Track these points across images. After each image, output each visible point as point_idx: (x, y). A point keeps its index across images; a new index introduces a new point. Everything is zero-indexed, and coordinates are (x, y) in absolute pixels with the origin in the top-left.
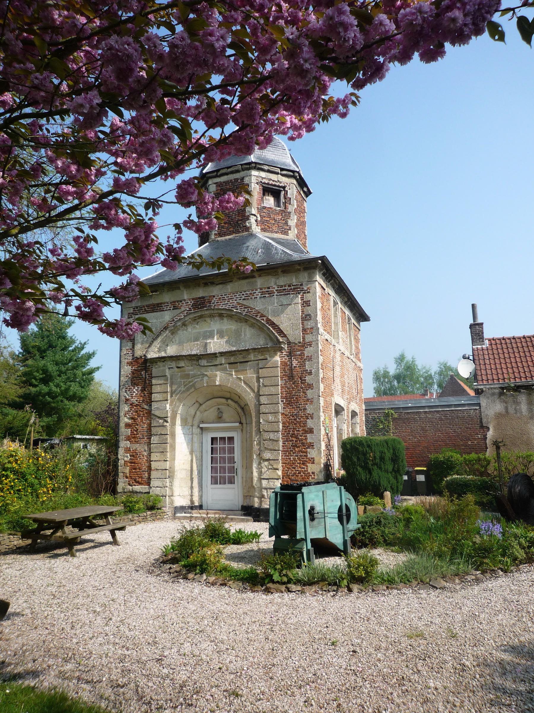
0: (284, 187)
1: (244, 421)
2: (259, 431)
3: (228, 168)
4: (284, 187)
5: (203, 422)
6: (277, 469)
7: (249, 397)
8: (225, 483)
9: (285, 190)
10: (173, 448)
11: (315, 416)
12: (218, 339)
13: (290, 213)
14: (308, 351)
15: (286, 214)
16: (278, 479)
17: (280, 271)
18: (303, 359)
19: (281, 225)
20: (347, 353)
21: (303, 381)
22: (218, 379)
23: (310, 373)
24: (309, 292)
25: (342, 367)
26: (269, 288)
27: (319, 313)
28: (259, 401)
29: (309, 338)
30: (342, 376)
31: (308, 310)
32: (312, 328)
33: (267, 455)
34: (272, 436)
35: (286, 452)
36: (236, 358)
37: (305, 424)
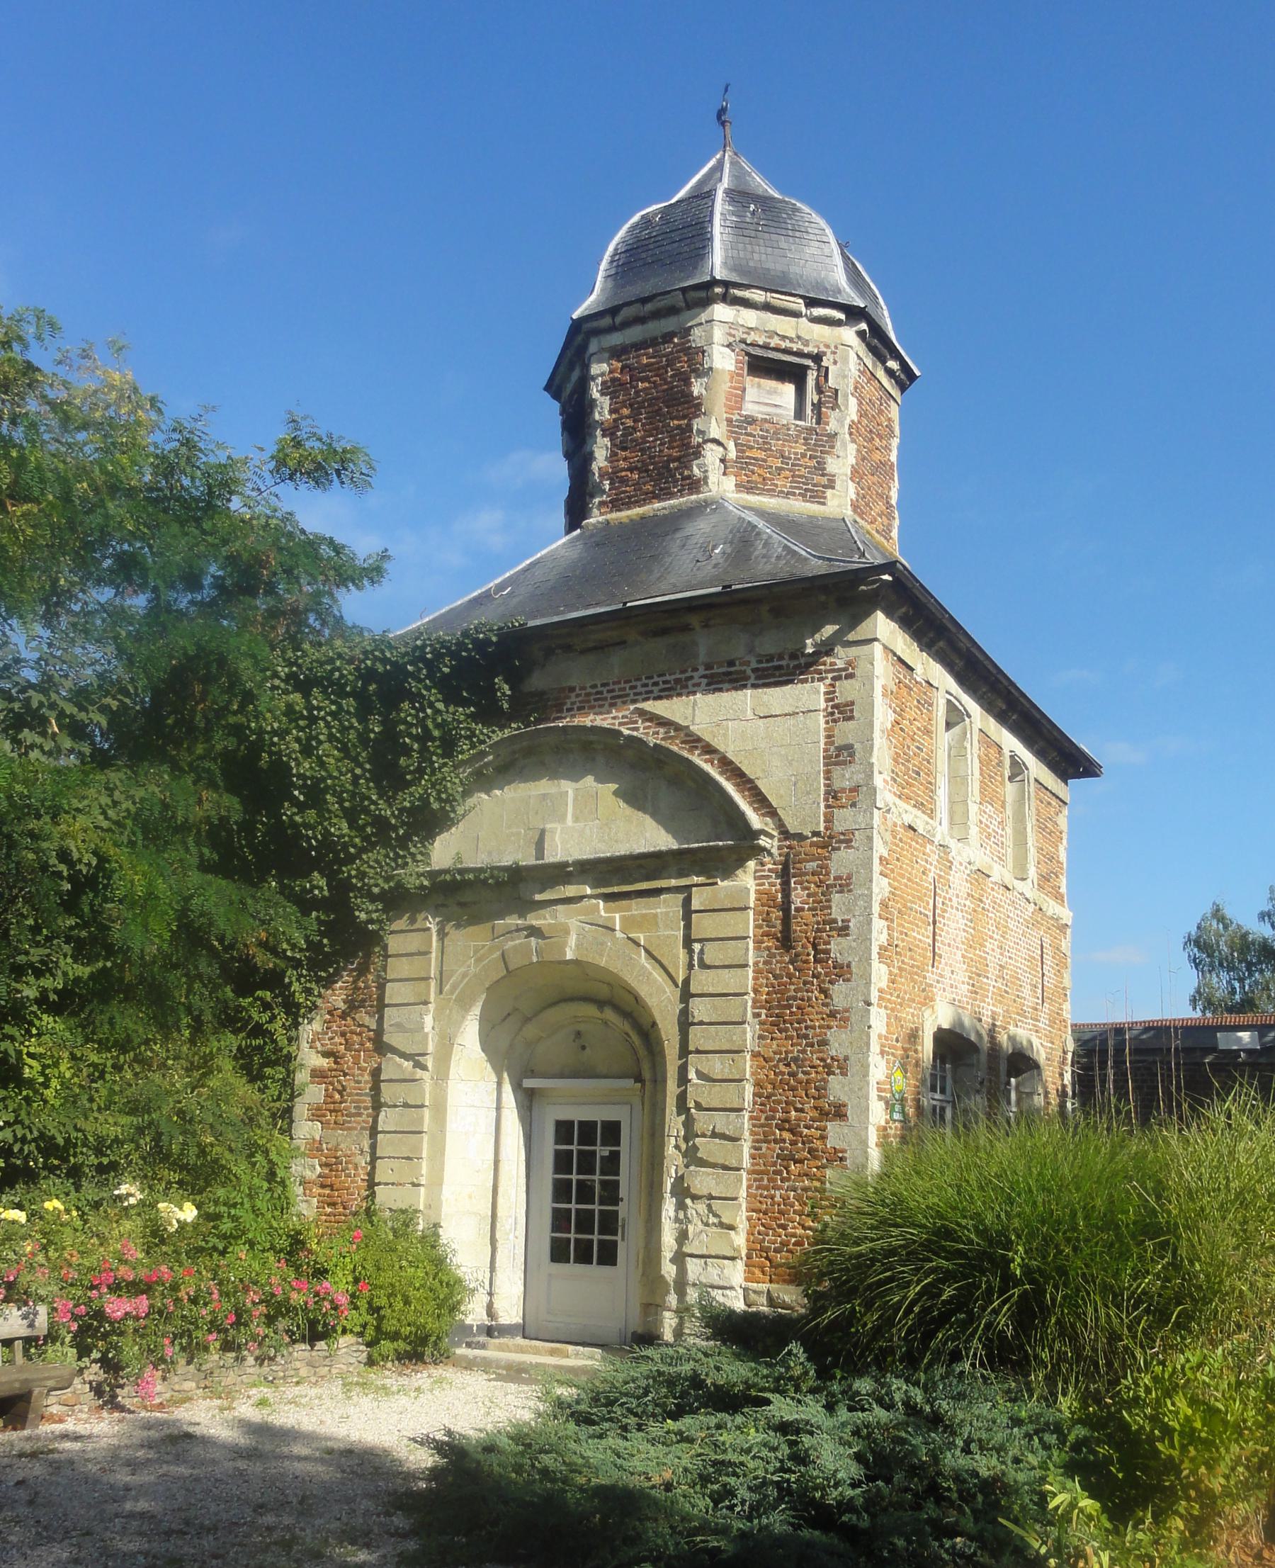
0: (817, 358)
1: (647, 1075)
2: (682, 1106)
3: (644, 301)
4: (817, 358)
5: (532, 1074)
6: (731, 1228)
7: (661, 1002)
11: (853, 1068)
12: (576, 819)
14: (841, 861)
15: (822, 443)
16: (733, 1259)
19: (803, 471)
20: (1000, 873)
21: (821, 955)
22: (572, 940)
23: (844, 930)
24: (850, 676)
25: (976, 916)
26: (731, 663)
27: (879, 740)
28: (685, 1013)
29: (845, 819)
30: (975, 941)
31: (847, 732)
32: (855, 789)
33: (703, 1181)
34: (720, 1122)
36: (619, 875)
37: (822, 1090)
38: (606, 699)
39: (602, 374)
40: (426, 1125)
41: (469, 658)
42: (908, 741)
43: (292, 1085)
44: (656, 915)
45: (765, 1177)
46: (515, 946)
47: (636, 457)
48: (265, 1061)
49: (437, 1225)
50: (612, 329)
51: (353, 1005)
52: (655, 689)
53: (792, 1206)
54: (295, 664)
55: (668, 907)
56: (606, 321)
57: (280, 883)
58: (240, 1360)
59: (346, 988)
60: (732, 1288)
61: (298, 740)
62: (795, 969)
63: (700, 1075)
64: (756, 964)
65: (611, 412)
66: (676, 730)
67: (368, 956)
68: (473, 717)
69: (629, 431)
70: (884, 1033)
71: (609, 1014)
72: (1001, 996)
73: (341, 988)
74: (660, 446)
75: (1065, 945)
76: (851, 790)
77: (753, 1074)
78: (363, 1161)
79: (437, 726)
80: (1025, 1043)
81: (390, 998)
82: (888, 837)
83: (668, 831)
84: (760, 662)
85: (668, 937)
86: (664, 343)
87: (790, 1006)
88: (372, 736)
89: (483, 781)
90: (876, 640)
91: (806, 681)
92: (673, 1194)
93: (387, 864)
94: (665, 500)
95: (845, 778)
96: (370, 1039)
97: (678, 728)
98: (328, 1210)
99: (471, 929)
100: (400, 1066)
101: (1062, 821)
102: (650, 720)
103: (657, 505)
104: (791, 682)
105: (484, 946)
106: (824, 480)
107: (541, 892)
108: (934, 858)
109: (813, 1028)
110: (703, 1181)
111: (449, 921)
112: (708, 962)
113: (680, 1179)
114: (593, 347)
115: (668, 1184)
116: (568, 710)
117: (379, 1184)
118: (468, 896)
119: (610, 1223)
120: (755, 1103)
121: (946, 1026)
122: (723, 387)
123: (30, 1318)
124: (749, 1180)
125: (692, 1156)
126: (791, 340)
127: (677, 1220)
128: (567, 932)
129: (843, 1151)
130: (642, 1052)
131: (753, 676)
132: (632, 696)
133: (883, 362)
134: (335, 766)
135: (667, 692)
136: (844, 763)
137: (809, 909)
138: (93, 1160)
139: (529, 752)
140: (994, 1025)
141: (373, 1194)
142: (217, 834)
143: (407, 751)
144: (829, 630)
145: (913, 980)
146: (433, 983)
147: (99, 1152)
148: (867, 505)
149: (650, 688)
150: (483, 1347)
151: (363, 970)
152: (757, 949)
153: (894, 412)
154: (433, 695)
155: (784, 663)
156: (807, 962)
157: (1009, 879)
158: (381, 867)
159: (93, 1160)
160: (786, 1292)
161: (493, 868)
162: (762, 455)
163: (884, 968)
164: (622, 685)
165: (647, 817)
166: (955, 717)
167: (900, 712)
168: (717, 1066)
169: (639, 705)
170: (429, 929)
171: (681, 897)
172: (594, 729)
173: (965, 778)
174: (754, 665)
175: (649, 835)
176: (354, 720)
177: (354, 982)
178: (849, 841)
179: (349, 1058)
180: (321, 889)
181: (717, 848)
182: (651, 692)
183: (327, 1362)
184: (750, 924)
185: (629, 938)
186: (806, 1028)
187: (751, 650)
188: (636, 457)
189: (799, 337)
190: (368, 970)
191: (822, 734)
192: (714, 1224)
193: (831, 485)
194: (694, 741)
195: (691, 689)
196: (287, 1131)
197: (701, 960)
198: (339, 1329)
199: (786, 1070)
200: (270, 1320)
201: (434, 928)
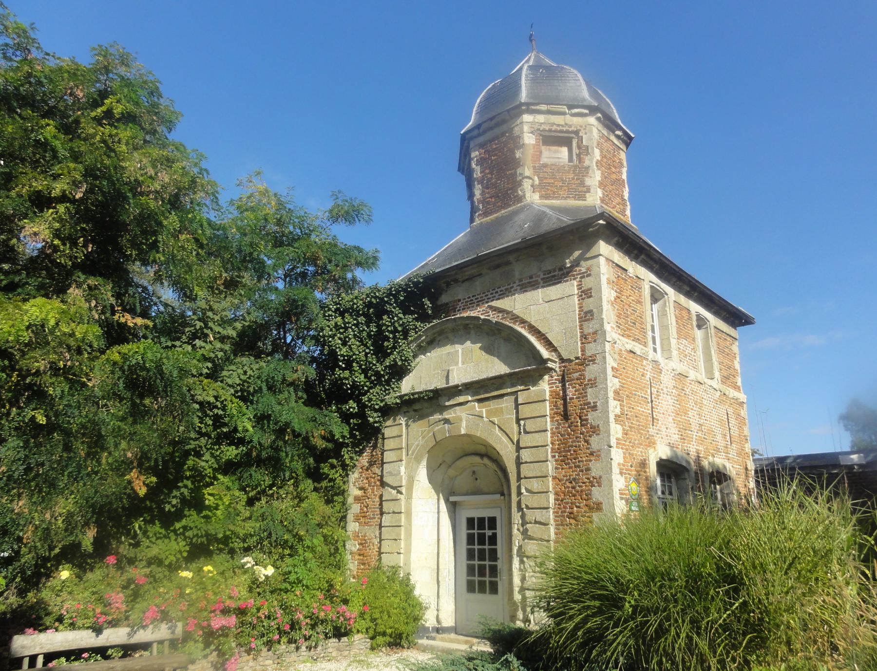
0: (577, 133)
1: (506, 492)
2: (520, 508)
3: (491, 119)
4: (577, 133)
5: (453, 494)
11: (604, 482)
12: (463, 363)
13: (588, 168)
14: (591, 371)
15: (582, 171)
18: (586, 384)
19: (574, 186)
21: (584, 422)
22: (464, 424)
24: (589, 275)
25: (681, 396)
26: (531, 277)
27: (606, 306)
28: (518, 458)
29: (591, 349)
30: (681, 412)
31: (589, 304)
32: (595, 333)
34: (538, 515)
36: (483, 389)
41: (412, 291)
42: (626, 307)
44: (502, 408)
48: (333, 495)
49: (409, 574)
50: (479, 135)
51: (371, 464)
52: (497, 295)
54: (339, 304)
55: (507, 403)
57: (337, 407)
58: (298, 648)
61: (340, 339)
63: (527, 490)
64: (552, 429)
67: (377, 439)
68: (416, 319)
69: (489, 180)
70: (622, 462)
71: (486, 461)
72: (701, 441)
75: (744, 412)
77: (554, 488)
78: (376, 541)
79: (400, 325)
80: (721, 466)
82: (617, 357)
83: (505, 364)
87: (570, 451)
89: (422, 350)
90: (600, 255)
91: (567, 281)
92: (517, 556)
97: (508, 312)
98: (362, 567)
100: (391, 493)
101: (735, 348)
103: (503, 212)
104: (560, 282)
107: (449, 400)
108: (649, 367)
109: (582, 461)
112: (528, 430)
113: (520, 547)
114: (472, 145)
115: (515, 550)
118: (417, 406)
121: (664, 457)
122: (530, 152)
123: (172, 629)
125: (525, 533)
126: (562, 126)
127: (520, 570)
128: (461, 420)
130: (503, 480)
134: (359, 351)
135: (502, 295)
136: (589, 320)
138: (241, 545)
140: (698, 457)
141: (380, 559)
142: (308, 386)
143: (387, 339)
144: (577, 254)
145: (640, 433)
146: (404, 451)
147: (244, 541)
148: (610, 199)
150: (434, 639)
151: (375, 447)
152: (552, 421)
153: (623, 156)
154: (397, 311)
156: (577, 426)
157: (702, 377)
159: (241, 545)
161: (426, 391)
162: (552, 181)
163: (619, 428)
166: (656, 296)
167: (620, 292)
168: (535, 485)
171: (513, 397)
172: (468, 317)
173: (667, 326)
174: (542, 276)
178: (593, 360)
179: (370, 490)
180: (354, 408)
181: (528, 371)
183: (348, 648)
187: (540, 269)
189: (566, 124)
191: (577, 307)
193: (588, 191)
194: (516, 318)
196: (344, 528)
197: (524, 429)
198: (355, 631)
199: (570, 485)
200: (313, 627)
201: (404, 423)
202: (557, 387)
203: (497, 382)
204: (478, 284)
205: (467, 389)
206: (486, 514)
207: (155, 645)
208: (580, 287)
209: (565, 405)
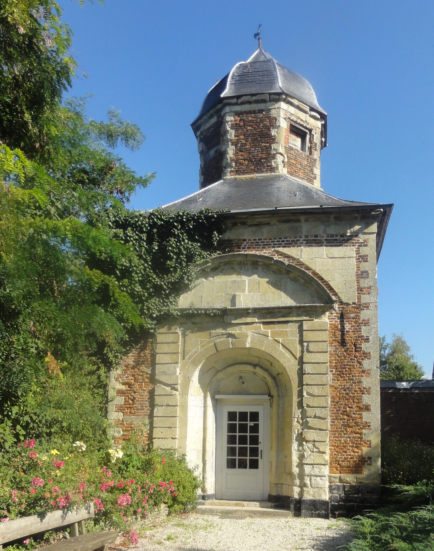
0: (310, 130)
1: (274, 392)
2: (300, 405)
3: (252, 95)
4: (310, 130)
5: (219, 393)
6: (324, 453)
7: (290, 365)
8: (245, 467)
9: (310, 134)
10: (184, 423)
12: (250, 292)
14: (364, 314)
16: (324, 465)
17: (332, 217)
18: (359, 324)
21: (357, 348)
22: (249, 340)
23: (367, 340)
24: (366, 246)
29: (365, 299)
32: (370, 288)
33: (310, 435)
35: (336, 433)
36: (270, 315)
37: (360, 400)
38: (260, 245)
39: (231, 121)
40: (178, 413)
43: (107, 397)
44: (286, 331)
45: (337, 433)
46: (221, 341)
47: (246, 155)
49: (184, 455)
50: (236, 104)
51: (138, 364)
52: (283, 243)
53: (349, 444)
56: (234, 101)
59: (134, 356)
60: (325, 476)
62: (347, 354)
63: (308, 394)
65: (235, 136)
66: (293, 260)
73: (132, 356)
74: (257, 152)
76: (368, 288)
78: (146, 429)
79: (185, 249)
81: (159, 360)
84: (328, 237)
85: (292, 340)
86: (258, 113)
87: (346, 368)
88: (154, 250)
89: (204, 273)
91: (347, 246)
93: (159, 305)
94: (260, 173)
95: (365, 283)
96: (147, 378)
99: (201, 333)
100: (165, 389)
102: (281, 255)
105: (205, 341)
106: (313, 176)
107: (236, 319)
109: (356, 376)
110: (310, 435)
111: (187, 330)
116: (243, 248)
117: (155, 438)
118: (197, 320)
119: (255, 452)
120: (332, 405)
124: (330, 434)
125: (305, 425)
127: (298, 450)
128: (247, 336)
129: (370, 423)
131: (325, 242)
132: (272, 245)
133: (322, 138)
135: (288, 245)
136: (365, 278)
137: (352, 332)
139: (226, 264)
141: (152, 443)
143: (171, 259)
144: (357, 227)
149: (281, 243)
150: (203, 504)
151: (142, 349)
155: (338, 238)
158: (157, 306)
160: (347, 477)
161: (213, 309)
164: (268, 240)
165: (282, 292)
168: (315, 390)
169: (276, 249)
170: (177, 333)
171: (297, 325)
172: (260, 256)
174: (325, 238)
175: (284, 300)
176: (145, 243)
177: (138, 354)
179: (137, 385)
181: (316, 307)
182: (281, 244)
184: (325, 336)
185: (275, 340)
186: (353, 376)
187: (324, 232)
188: (246, 155)
189: (306, 121)
190: (146, 349)
192: (316, 452)
195: (299, 244)
199: (344, 392)
201: (180, 333)
202: (336, 322)
203: (286, 311)
204: (265, 230)
205: (255, 312)
206: (249, 409)
207: (76, 525)
208: (358, 252)
209: (343, 335)
